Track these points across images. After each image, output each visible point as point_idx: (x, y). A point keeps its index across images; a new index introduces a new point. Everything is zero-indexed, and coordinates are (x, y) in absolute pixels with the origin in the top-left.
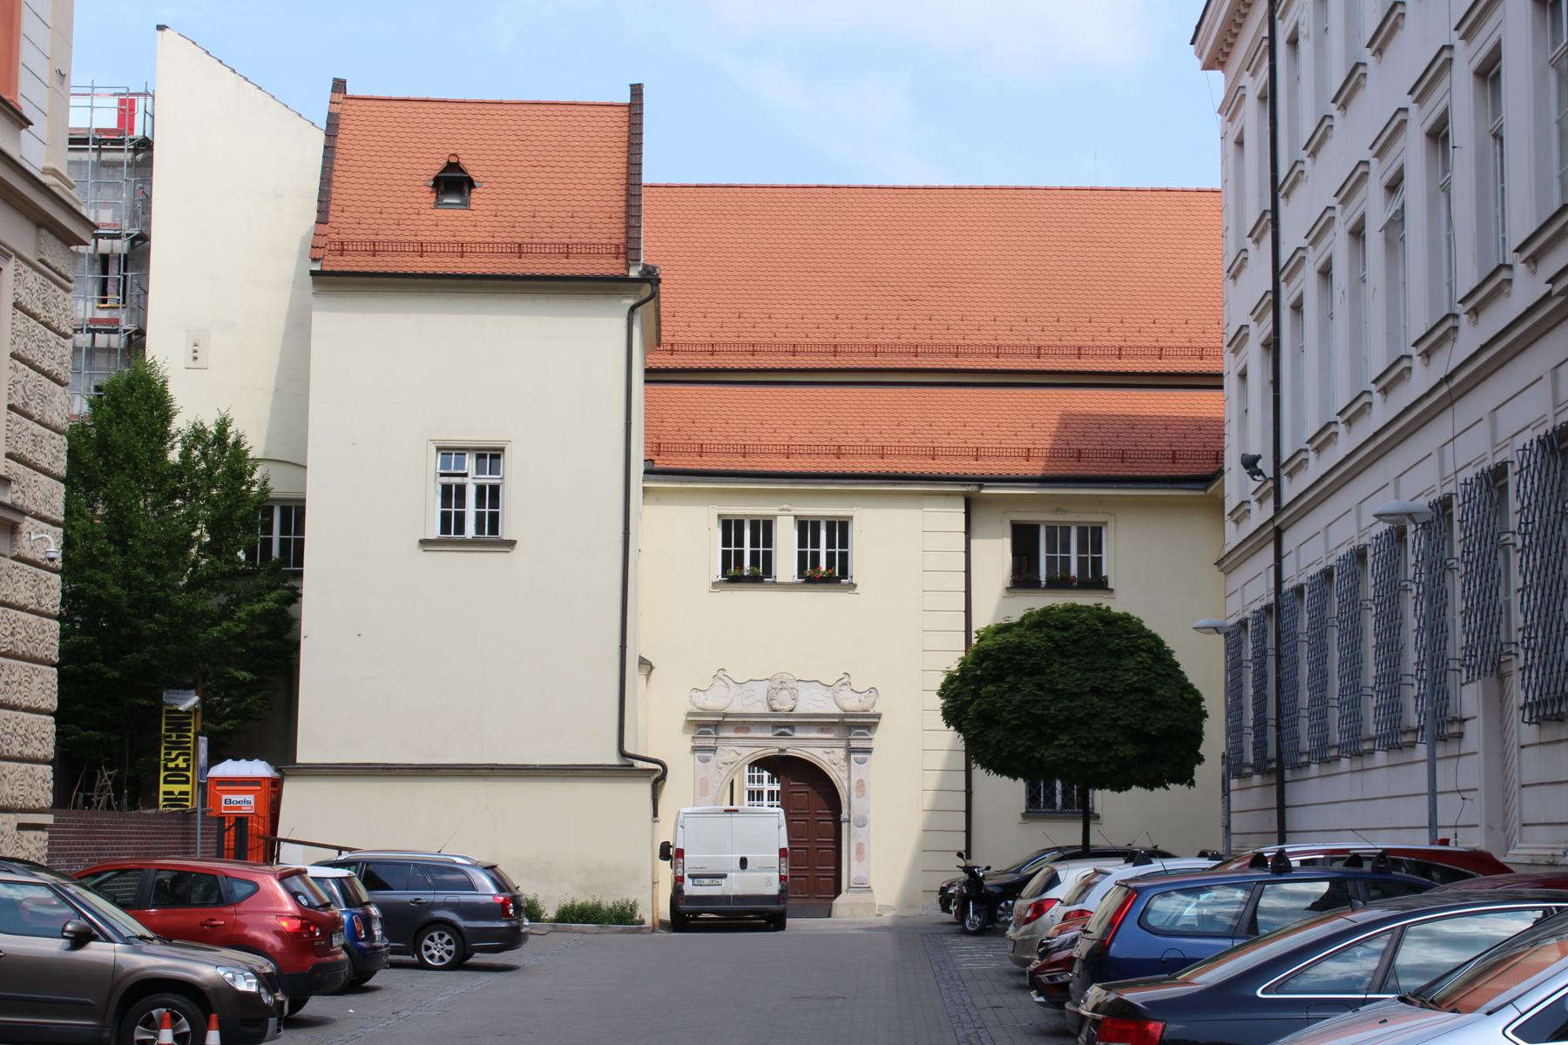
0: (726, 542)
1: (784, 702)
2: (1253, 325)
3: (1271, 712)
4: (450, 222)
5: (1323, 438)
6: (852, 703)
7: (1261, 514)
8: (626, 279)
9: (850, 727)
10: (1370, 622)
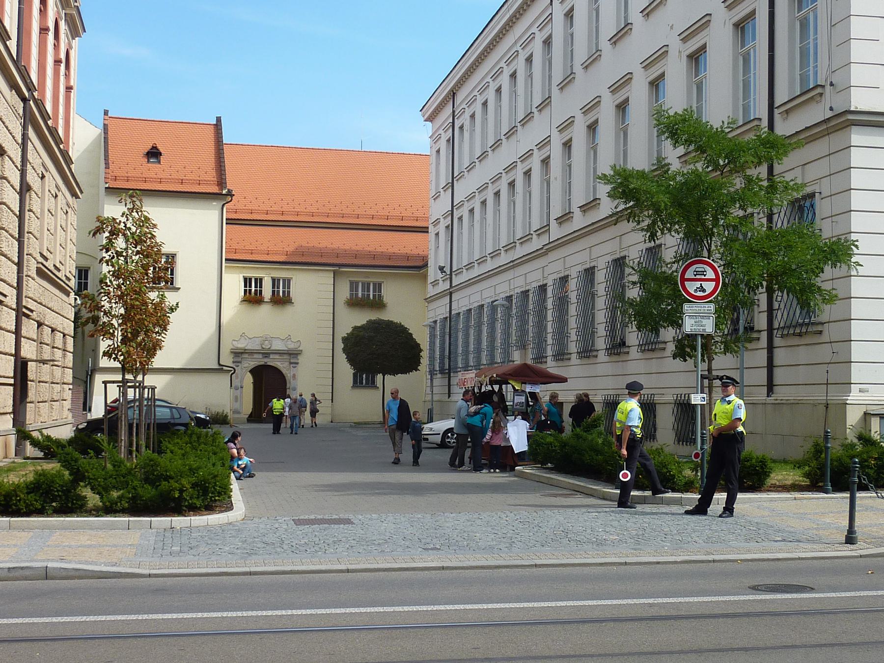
0: (245, 286)
1: (267, 345)
2: (442, 220)
3: (447, 353)
4: (153, 169)
5: (470, 266)
6: (291, 346)
7: (444, 286)
8: (221, 194)
9: (290, 354)
10: (485, 329)
